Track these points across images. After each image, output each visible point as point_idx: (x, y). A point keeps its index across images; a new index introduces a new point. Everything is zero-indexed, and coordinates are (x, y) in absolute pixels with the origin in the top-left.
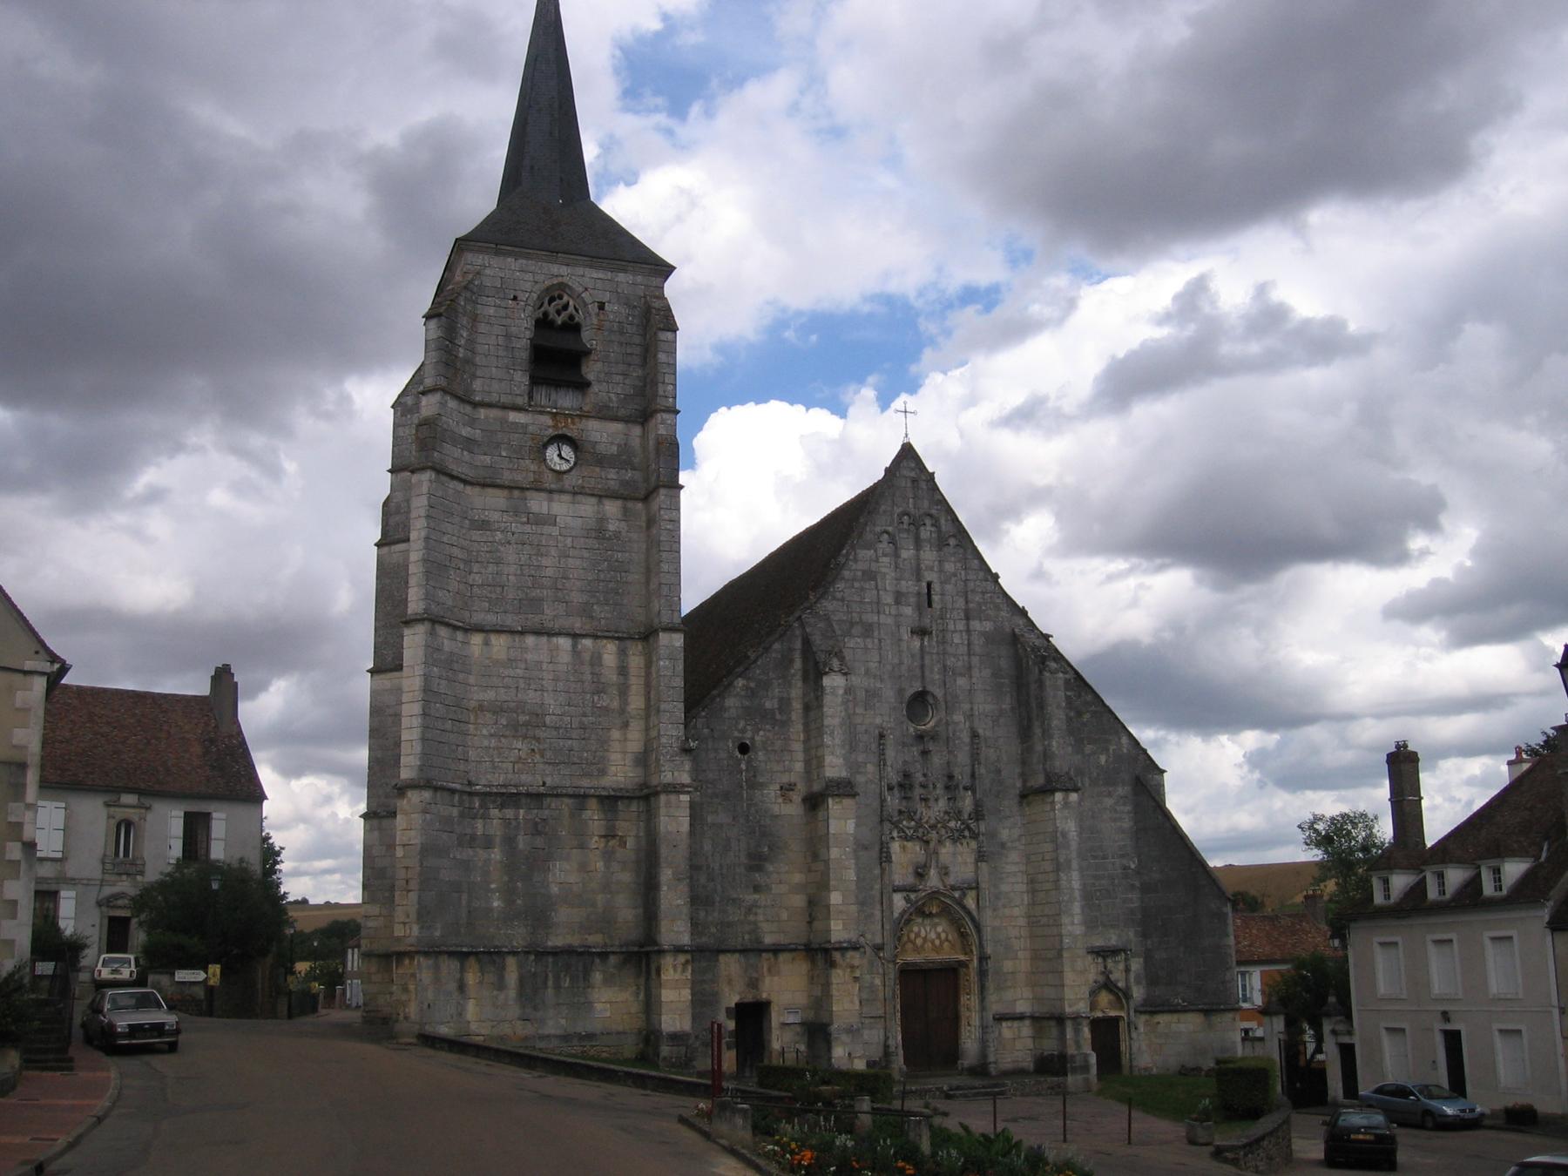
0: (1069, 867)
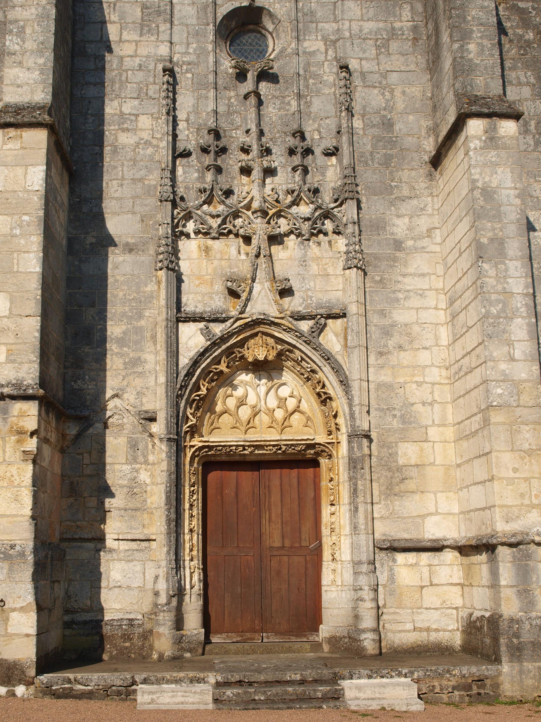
0: (502, 254)
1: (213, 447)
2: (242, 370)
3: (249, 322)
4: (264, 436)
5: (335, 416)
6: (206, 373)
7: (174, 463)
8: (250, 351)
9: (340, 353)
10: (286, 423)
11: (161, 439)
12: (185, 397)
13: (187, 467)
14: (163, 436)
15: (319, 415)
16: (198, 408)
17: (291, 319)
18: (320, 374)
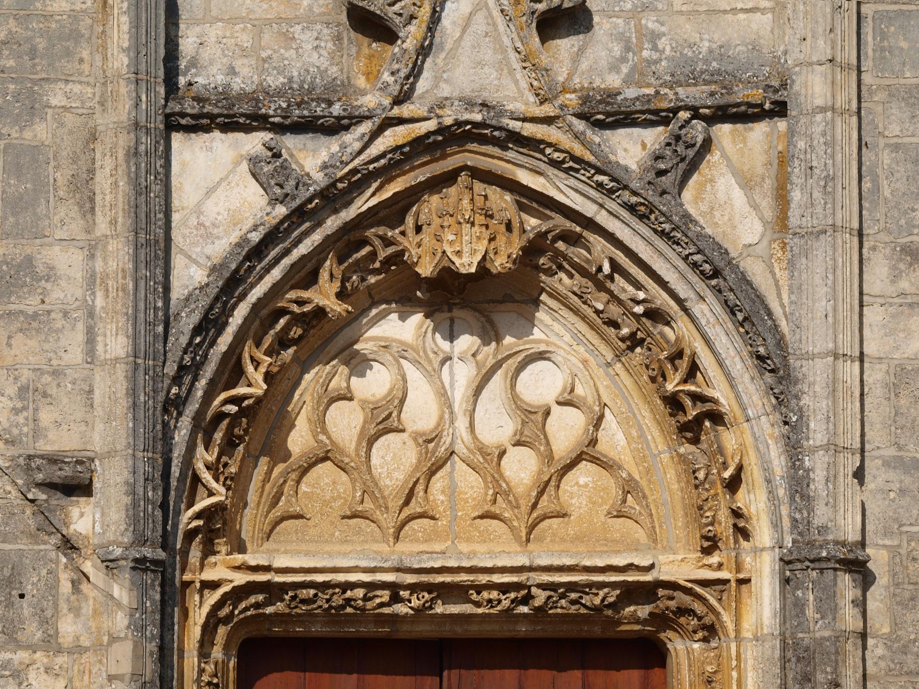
1: (284, 587)
2: (388, 302)
3: (428, 134)
4: (464, 547)
5: (733, 484)
6: (266, 314)
7: (153, 646)
8: (426, 236)
9: (759, 250)
10: (544, 501)
11: (110, 564)
12: (192, 407)
13: (191, 660)
14: (118, 552)
15: (671, 475)
16: (229, 445)
17: (580, 125)
18: (683, 325)
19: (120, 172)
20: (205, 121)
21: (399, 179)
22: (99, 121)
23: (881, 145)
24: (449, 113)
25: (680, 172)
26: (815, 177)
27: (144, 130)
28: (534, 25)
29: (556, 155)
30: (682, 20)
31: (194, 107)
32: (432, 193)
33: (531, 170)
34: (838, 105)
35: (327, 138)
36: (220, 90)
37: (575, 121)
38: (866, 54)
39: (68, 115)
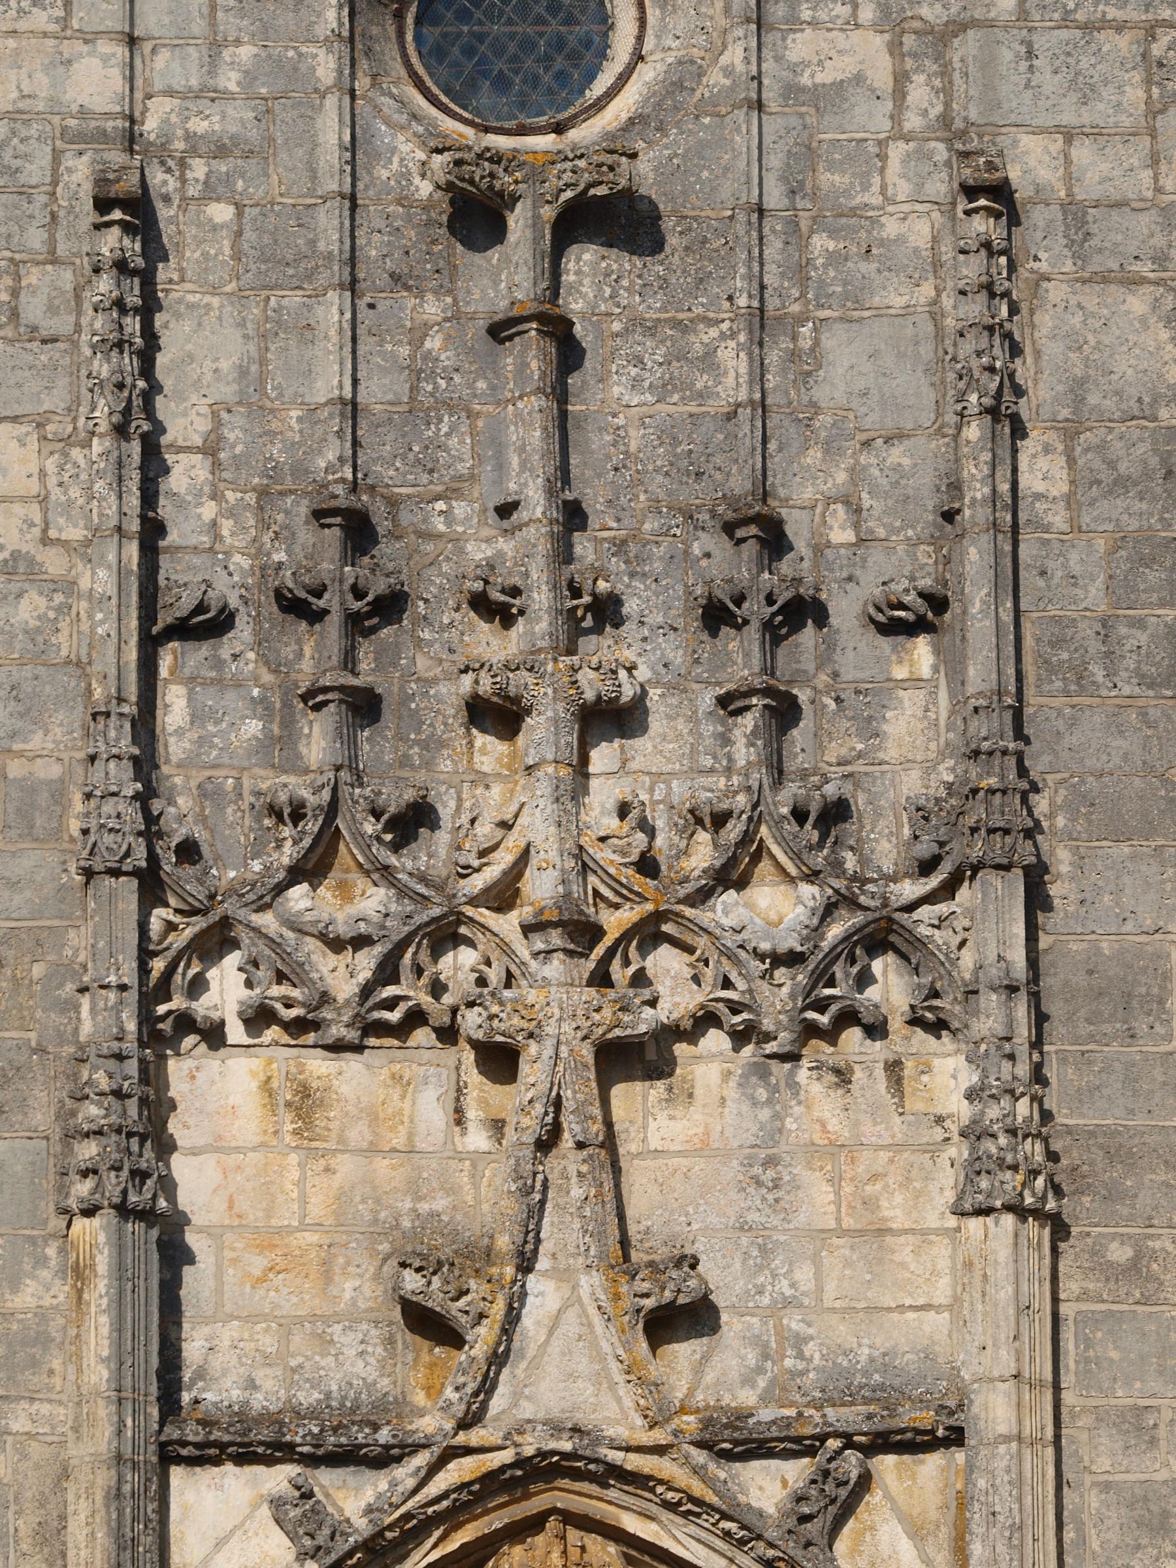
3: (503, 1468)
17: (700, 1457)
19: (98, 1520)
20: (212, 1451)
21: (469, 1526)
22: (73, 1452)
23: (1088, 1483)
24: (531, 1440)
25: (830, 1518)
26: (999, 1525)
27: (129, 1464)
28: (640, 1326)
29: (670, 1495)
30: (834, 1319)
31: (197, 1434)
32: (513, 1543)
33: (640, 1514)
34: (1026, 1432)
35: (374, 1472)
36: (236, 1408)
37: (694, 1451)
38: (1067, 1366)
39: (33, 1444)
